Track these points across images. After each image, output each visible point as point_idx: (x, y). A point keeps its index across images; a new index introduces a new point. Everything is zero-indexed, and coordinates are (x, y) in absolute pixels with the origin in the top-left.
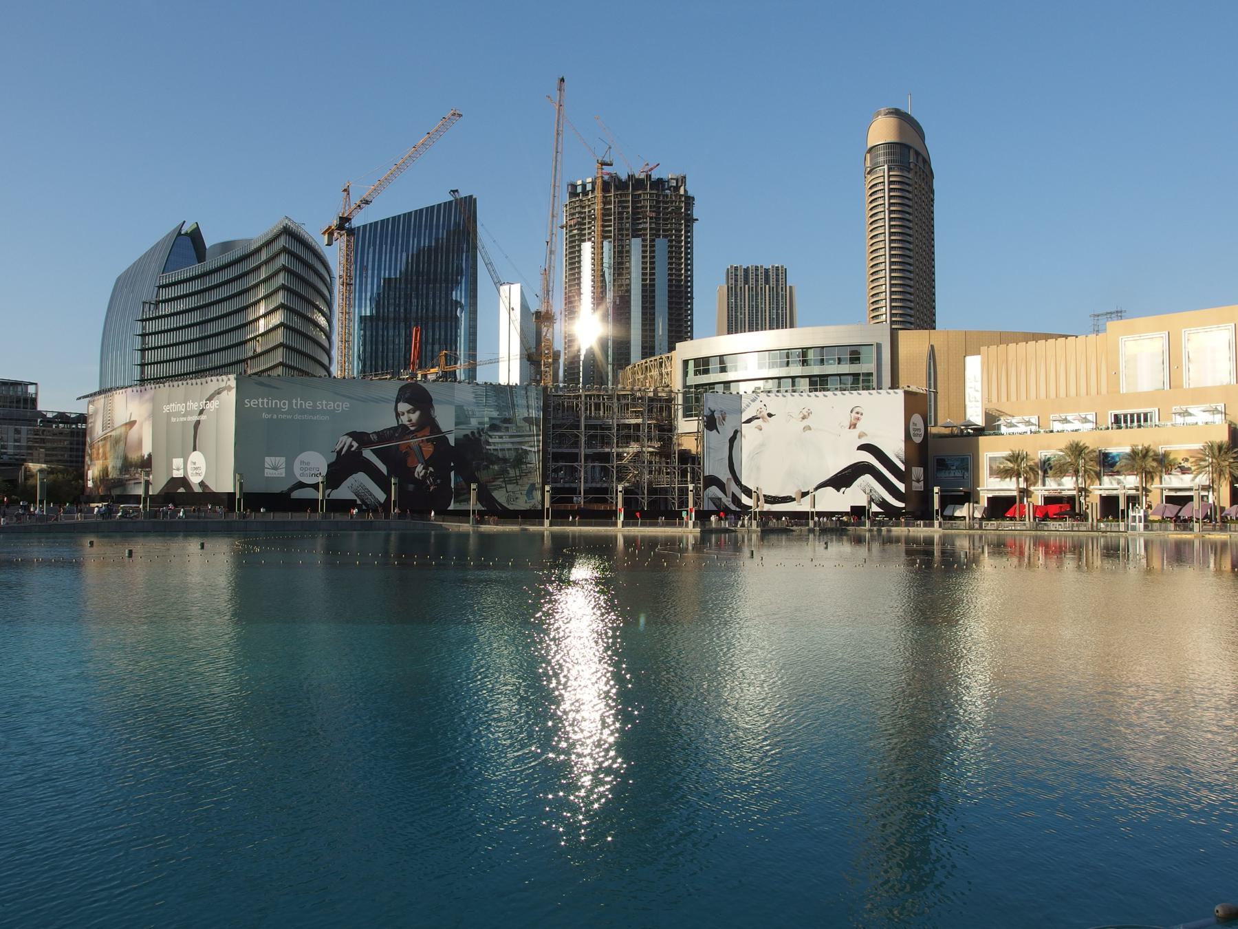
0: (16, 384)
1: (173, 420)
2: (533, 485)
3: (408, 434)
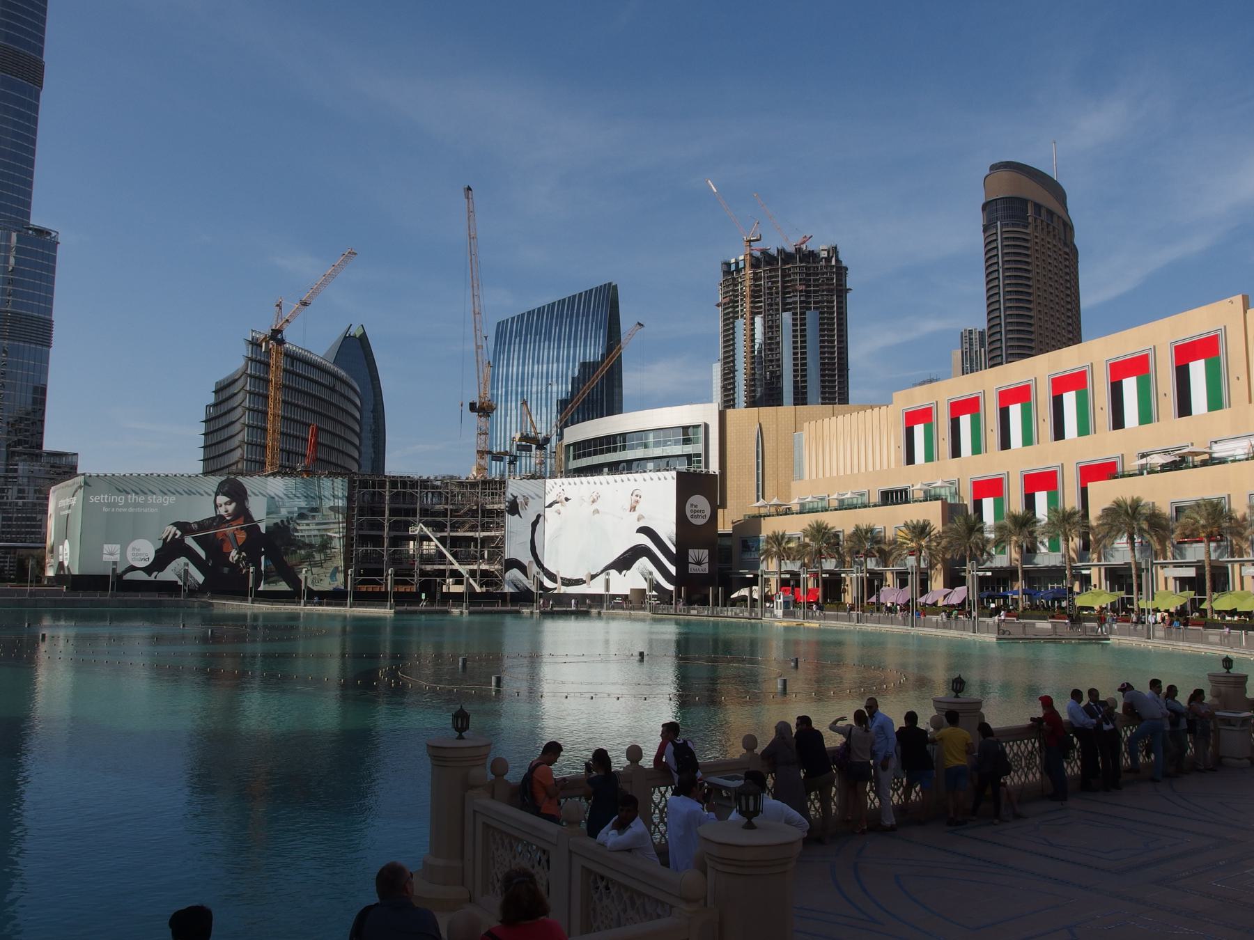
2: (337, 568)
3: (224, 523)
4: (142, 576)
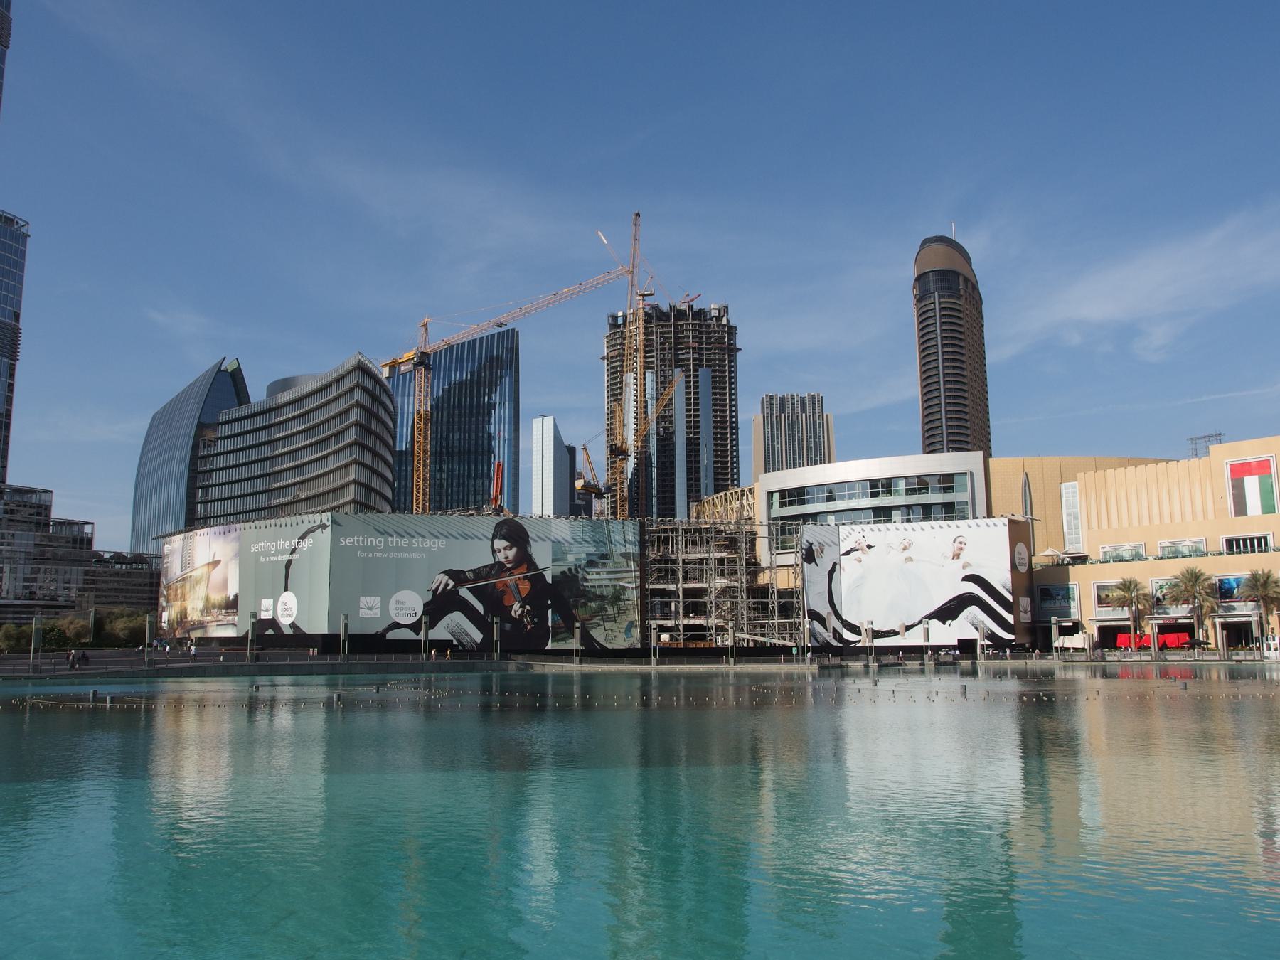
0: (72, 524)
1: (262, 559)
2: (631, 623)
3: (505, 572)
4: (408, 635)
